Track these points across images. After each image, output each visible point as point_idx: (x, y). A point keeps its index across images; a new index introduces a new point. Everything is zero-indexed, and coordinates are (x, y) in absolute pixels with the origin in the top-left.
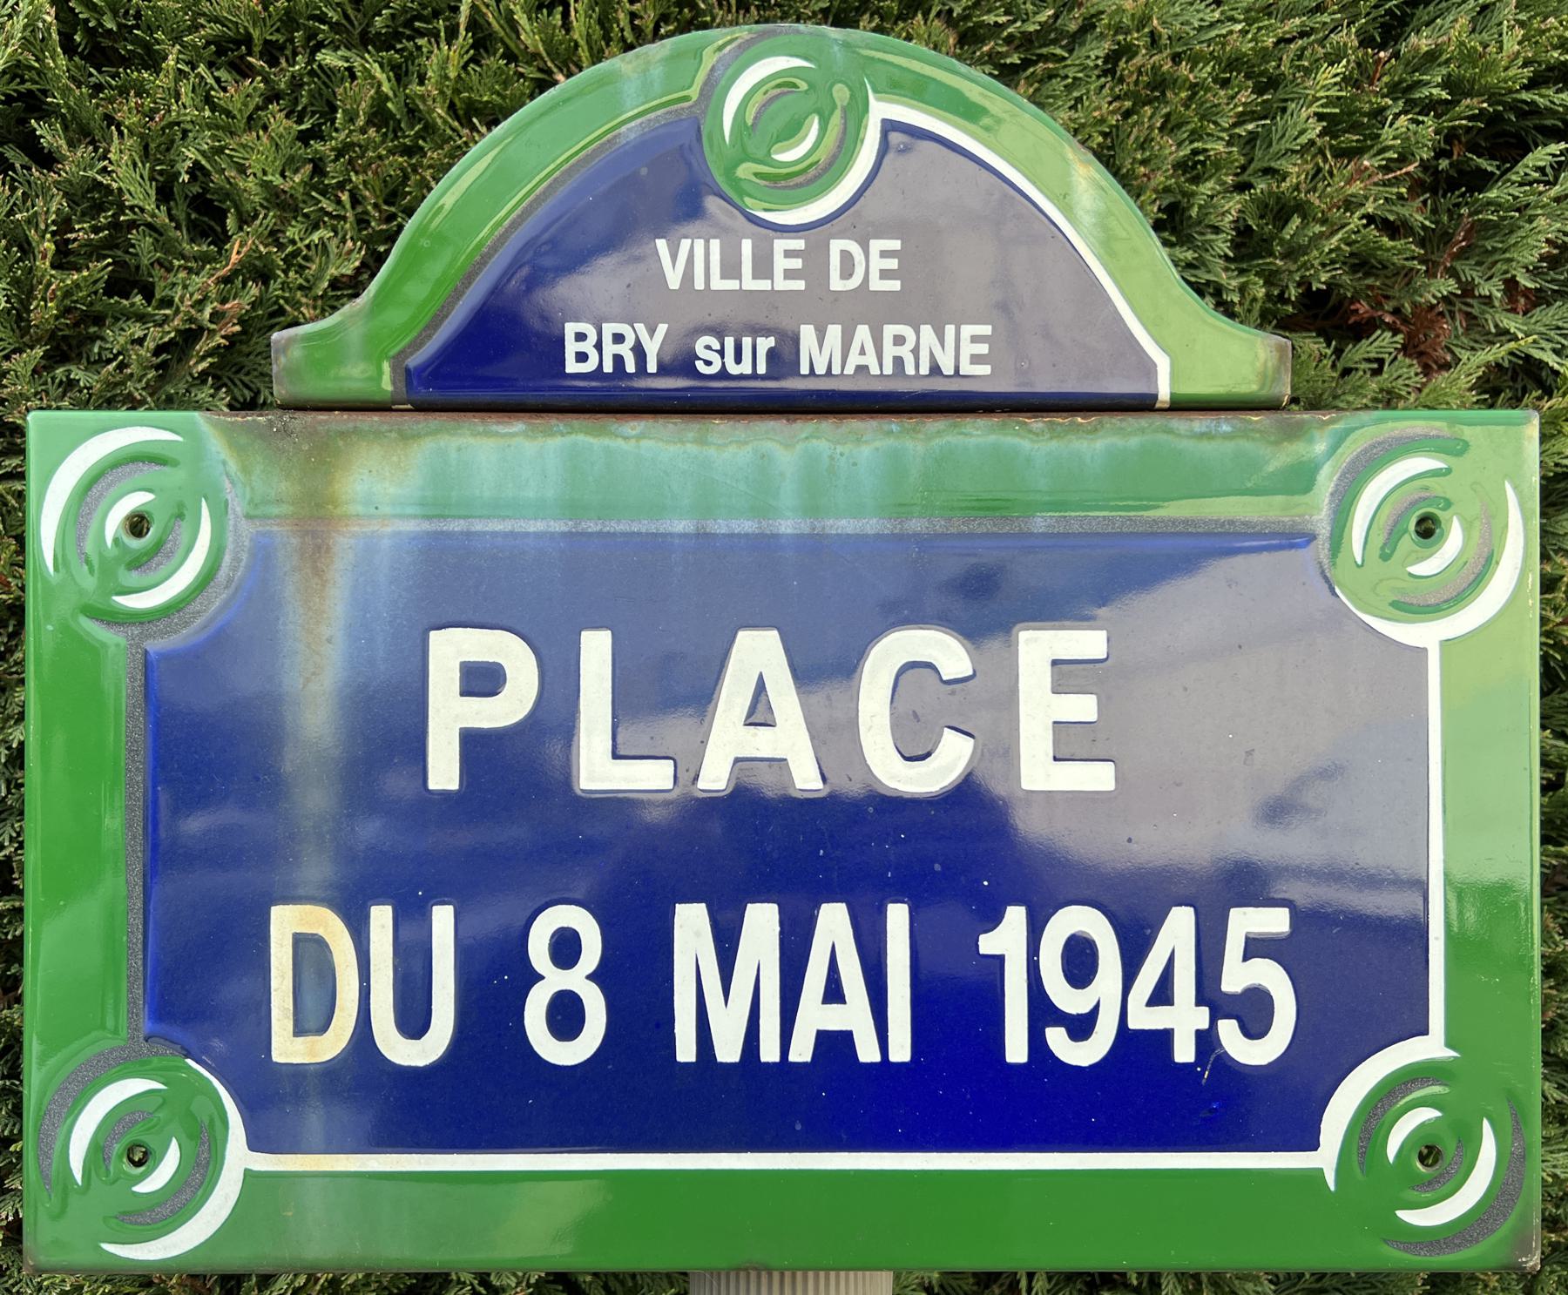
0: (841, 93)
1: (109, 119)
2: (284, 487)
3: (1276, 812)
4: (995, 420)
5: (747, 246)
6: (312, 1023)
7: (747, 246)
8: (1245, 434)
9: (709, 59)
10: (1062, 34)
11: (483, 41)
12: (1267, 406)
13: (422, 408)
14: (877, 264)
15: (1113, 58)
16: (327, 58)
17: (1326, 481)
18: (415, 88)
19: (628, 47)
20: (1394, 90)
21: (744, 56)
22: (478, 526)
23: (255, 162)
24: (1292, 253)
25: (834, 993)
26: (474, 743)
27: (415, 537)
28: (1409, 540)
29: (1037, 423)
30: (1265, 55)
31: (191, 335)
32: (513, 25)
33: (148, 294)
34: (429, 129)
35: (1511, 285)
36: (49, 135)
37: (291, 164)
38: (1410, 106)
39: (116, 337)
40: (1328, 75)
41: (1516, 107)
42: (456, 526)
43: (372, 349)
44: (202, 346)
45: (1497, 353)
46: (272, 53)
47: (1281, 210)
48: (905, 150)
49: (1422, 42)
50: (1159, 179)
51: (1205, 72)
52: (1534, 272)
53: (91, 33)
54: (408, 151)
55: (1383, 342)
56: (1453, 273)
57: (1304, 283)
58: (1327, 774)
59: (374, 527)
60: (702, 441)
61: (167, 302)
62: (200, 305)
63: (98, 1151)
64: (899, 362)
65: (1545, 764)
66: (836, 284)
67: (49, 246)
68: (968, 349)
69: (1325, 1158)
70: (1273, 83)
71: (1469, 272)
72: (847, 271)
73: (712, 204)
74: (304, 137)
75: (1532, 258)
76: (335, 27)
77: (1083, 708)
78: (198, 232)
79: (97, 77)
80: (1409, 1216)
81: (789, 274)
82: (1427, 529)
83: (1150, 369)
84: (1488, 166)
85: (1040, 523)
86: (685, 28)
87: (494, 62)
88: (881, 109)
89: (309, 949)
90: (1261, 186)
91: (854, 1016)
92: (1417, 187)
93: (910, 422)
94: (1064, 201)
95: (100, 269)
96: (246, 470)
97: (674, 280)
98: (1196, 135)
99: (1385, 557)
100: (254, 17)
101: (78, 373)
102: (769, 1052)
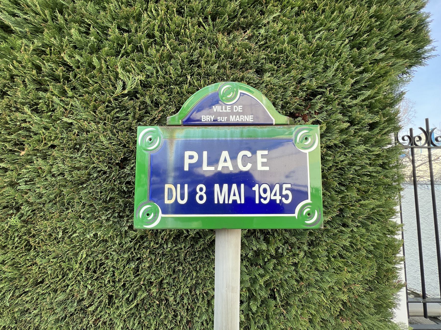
0: (235, 89)
1: (146, 94)
2: (168, 135)
3: (287, 177)
4: (254, 126)
5: (224, 107)
6: (170, 198)
7: (224, 107)
8: (284, 128)
9: (220, 86)
10: (260, 83)
11: (190, 84)
12: (287, 125)
13: (184, 126)
14: (239, 109)
15: (266, 86)
16: (172, 86)
17: (294, 133)
18: (182, 90)
19: (208, 85)
20: (300, 89)
21: (224, 85)
22: (191, 139)
23: (163, 98)
24: (288, 108)
25: (234, 195)
26: (190, 164)
27: (184, 140)
28: (304, 140)
29: (259, 127)
30: (284, 85)
31: (154, 119)
32: (194, 82)
33: (149, 114)
34: (184, 94)
35: (315, 112)
36: (138, 96)
37: (167, 99)
38: (302, 91)
39: (145, 119)
40: (292, 88)
41: (315, 91)
42: (188, 139)
43: (179, 119)
44: (156, 120)
45: (314, 120)
46: (165, 86)
47: (287, 103)
48: (243, 96)
49: (303, 84)
50: (272, 99)
51: (277, 87)
52: (318, 110)
53: (144, 84)
54: (181, 97)
55: (300, 118)
56: (308, 110)
57: (290, 111)
58: (294, 172)
59: (178, 139)
60: (218, 129)
61: (152, 115)
62: (156, 115)
63: (143, 214)
64: (242, 120)
65: (322, 169)
66: (234, 111)
67: (138, 108)
68: (250, 118)
69: (296, 215)
70: (286, 88)
71: (310, 110)
72: (236, 109)
73: (220, 102)
74: (169, 96)
75: (318, 108)
76: (173, 83)
77: (265, 160)
78: (155, 107)
79: (144, 89)
80: (307, 222)
81: (229, 110)
82: (306, 139)
83: (272, 120)
84: (312, 98)
85: (259, 138)
86: (214, 83)
87: (192, 87)
88: (240, 91)
89: (170, 190)
90: (284, 100)
91: (237, 198)
92: (303, 100)
93: (244, 127)
94: (262, 101)
95: (144, 111)
96: (163, 133)
97: (215, 111)
98: (276, 94)
99: (301, 142)
100: (163, 82)
101: (141, 123)
102: (226, 202)
